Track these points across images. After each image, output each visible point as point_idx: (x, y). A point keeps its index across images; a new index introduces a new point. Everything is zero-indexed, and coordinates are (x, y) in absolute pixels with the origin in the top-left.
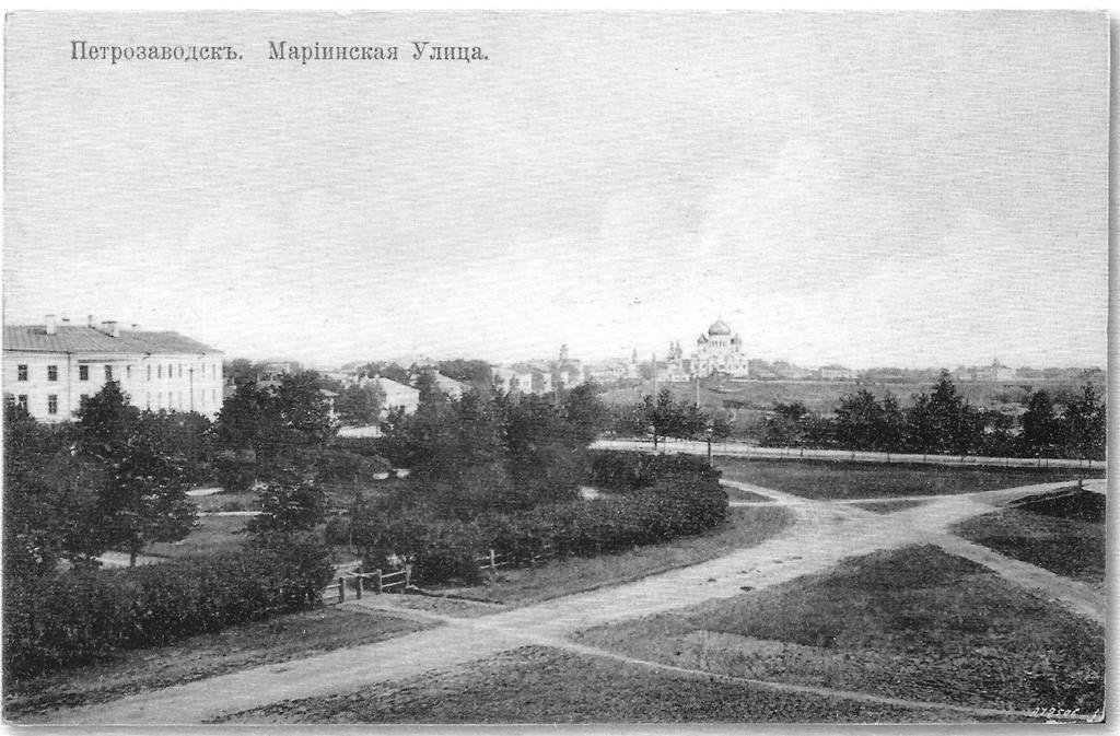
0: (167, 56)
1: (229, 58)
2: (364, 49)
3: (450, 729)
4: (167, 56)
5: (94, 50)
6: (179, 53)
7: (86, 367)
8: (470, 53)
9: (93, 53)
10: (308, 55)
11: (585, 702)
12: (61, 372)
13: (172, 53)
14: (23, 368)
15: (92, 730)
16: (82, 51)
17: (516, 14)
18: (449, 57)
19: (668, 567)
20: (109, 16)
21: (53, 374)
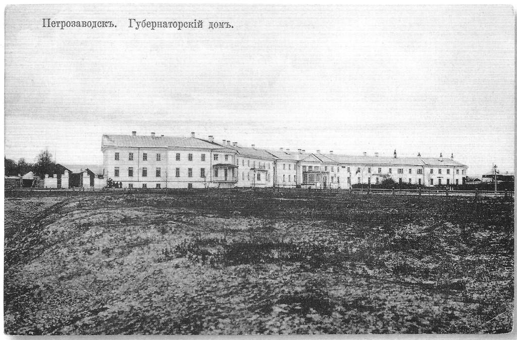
0: (84, 25)
4: (84, 25)
5: (149, 23)
6: (89, 25)
13: (86, 24)
14: (440, 170)
15: (516, 321)
16: (49, 23)
21: (190, 158)
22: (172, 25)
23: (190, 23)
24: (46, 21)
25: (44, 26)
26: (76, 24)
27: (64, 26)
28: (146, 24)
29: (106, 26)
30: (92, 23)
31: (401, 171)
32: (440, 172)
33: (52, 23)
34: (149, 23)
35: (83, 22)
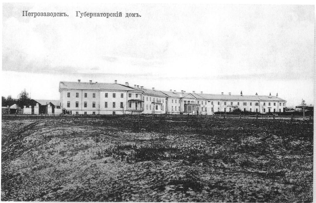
0: (49, 15)
1: (137, 16)
2: (114, 14)
4: (49, 15)
5: (29, 13)
6: (52, 15)
7: (131, 94)
9: (30, 14)
11: (195, 197)
12: (80, 95)
13: (50, 14)
23: (114, 14)
24: (25, 13)
27: (92, 16)
28: (87, 14)
30: (53, 14)
31: (245, 104)
32: (270, 104)
35: (48, 13)
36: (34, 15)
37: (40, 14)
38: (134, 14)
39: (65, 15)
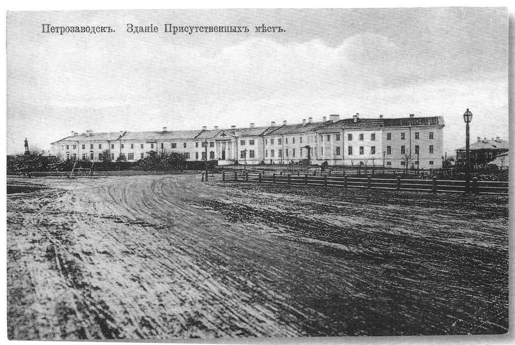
0: (83, 31)
1: (109, 31)
2: (102, 27)
3: (120, 342)
5: (156, 28)
6: (88, 30)
7: (273, 140)
8: (138, 29)
10: (150, 28)
12: (407, 136)
13: (85, 29)
14: (185, 144)
16: (49, 29)
17: (430, 9)
18: (147, 31)
19: (97, 342)
20: (183, 12)
22: (198, 30)
24: (168, 27)
25: (43, 32)
26: (75, 29)
27: (63, 31)
29: (105, 31)
30: (91, 28)
31: (174, 146)
32: (92, 147)
33: (154, 29)
34: (216, 28)
35: (82, 28)
36: (59, 30)
37: (69, 29)
38: (259, 27)
39: (110, 30)
